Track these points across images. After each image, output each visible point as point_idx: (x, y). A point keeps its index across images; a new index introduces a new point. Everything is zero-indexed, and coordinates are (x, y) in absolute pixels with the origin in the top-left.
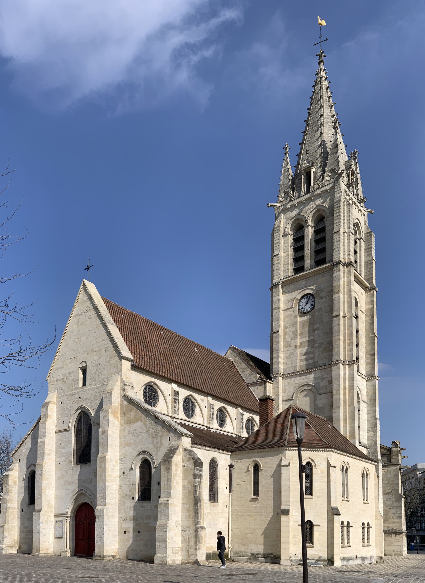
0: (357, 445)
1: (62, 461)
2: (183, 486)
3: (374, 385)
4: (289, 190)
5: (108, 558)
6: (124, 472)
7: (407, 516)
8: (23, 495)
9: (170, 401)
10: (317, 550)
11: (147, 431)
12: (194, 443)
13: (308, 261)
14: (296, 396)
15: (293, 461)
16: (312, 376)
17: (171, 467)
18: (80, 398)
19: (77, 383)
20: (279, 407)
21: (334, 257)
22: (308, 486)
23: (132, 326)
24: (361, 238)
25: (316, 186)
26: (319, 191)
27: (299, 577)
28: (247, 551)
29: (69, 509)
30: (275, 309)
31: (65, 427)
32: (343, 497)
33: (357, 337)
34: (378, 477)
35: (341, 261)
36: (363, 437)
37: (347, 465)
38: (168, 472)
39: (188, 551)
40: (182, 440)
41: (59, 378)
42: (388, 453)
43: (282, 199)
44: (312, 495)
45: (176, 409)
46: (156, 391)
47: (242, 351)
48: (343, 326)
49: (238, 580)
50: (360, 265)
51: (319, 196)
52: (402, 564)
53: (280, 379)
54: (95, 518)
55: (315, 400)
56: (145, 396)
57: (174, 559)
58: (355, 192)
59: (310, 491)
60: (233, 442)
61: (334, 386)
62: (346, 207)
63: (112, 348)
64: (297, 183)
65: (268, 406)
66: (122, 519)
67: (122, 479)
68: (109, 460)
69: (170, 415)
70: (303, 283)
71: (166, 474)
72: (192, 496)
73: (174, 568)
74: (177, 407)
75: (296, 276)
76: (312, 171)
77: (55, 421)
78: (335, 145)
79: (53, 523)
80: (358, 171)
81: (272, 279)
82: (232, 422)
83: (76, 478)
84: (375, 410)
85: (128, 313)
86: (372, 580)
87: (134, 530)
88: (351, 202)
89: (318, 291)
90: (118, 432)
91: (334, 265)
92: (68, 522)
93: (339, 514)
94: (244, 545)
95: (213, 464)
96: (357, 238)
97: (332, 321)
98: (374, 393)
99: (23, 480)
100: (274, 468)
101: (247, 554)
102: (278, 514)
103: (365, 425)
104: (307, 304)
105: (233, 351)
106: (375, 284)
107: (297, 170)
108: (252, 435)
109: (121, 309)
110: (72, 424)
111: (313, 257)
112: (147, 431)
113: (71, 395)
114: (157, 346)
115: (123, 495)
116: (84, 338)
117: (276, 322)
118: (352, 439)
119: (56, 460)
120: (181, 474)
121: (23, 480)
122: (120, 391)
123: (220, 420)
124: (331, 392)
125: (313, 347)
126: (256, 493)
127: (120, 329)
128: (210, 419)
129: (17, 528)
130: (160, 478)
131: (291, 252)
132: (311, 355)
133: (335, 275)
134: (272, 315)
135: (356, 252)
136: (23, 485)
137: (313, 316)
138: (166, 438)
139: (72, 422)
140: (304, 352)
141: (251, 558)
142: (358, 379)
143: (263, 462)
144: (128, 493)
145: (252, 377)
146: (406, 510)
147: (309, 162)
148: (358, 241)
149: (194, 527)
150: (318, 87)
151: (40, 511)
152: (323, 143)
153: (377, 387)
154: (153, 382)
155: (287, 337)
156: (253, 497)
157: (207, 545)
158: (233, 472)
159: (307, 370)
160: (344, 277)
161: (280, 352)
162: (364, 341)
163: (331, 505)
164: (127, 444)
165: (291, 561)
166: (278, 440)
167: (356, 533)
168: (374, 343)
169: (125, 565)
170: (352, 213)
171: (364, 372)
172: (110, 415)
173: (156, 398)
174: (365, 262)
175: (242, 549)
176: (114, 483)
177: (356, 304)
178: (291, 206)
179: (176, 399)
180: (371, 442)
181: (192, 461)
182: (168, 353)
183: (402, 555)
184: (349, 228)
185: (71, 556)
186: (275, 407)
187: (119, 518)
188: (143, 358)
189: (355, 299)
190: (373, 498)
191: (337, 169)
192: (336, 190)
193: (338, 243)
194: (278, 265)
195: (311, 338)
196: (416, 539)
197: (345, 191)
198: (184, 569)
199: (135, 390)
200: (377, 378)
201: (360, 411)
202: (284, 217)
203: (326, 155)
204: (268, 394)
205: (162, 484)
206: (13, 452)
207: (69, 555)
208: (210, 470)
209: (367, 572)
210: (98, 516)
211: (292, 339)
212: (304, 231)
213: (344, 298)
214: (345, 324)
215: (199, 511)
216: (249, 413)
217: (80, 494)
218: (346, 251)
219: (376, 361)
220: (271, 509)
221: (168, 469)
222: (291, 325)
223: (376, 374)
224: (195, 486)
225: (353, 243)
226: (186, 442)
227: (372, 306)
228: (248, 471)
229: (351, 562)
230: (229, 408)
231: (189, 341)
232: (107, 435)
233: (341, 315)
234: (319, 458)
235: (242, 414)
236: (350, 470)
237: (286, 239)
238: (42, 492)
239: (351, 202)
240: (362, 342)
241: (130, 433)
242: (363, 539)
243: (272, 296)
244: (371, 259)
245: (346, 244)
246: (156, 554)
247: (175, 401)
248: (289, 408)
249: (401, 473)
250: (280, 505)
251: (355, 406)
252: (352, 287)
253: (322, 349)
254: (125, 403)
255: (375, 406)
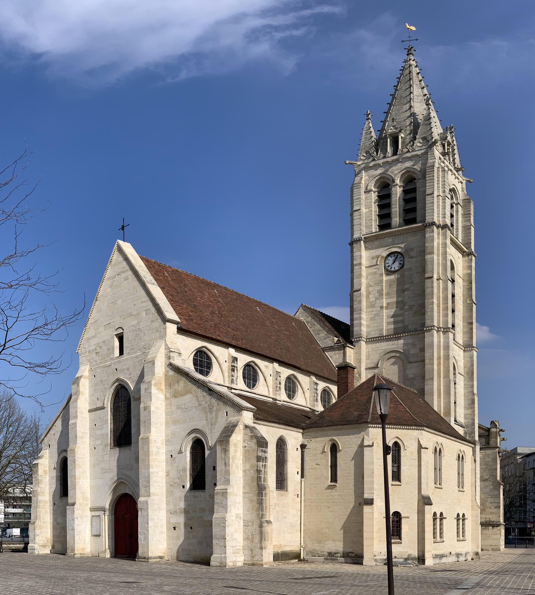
0: (452, 423)
1: (97, 445)
2: (244, 471)
3: (472, 357)
4: (373, 150)
5: (154, 560)
6: (172, 456)
7: (505, 506)
8: (54, 486)
9: (227, 369)
10: (406, 547)
11: (199, 405)
12: (257, 418)
13: (395, 219)
14: (382, 364)
15: (378, 441)
16: (401, 342)
17: (229, 448)
18: (116, 369)
19: (113, 353)
20: (362, 376)
21: (427, 218)
22: (395, 470)
23: (178, 284)
24: (458, 203)
25: (405, 150)
26: (408, 155)
27: (384, 579)
28: (322, 550)
29: (107, 502)
30: (356, 265)
31: (99, 405)
32: (435, 483)
33: (453, 302)
34: (475, 461)
35: (434, 222)
36: (459, 415)
37: (440, 446)
38: (225, 455)
39: (252, 550)
40: (242, 415)
41: (91, 348)
42: (487, 434)
43: (362, 158)
44: (400, 481)
45: (234, 378)
46: (209, 358)
47: (316, 311)
48: (437, 291)
49: (312, 584)
50: (457, 229)
51: (409, 159)
52: (500, 559)
53: (363, 344)
54: (137, 511)
55: (405, 369)
56: (195, 364)
57: (234, 560)
58: (451, 161)
59: (397, 476)
60: (306, 416)
61: (427, 355)
62: (440, 172)
63: (153, 310)
64: (381, 145)
65: (347, 374)
66: (171, 512)
67: (169, 464)
68: (153, 441)
69: (227, 385)
70: (390, 240)
71: (223, 456)
72: (256, 483)
73: (235, 571)
74: (235, 376)
75: (381, 233)
76: (400, 137)
77: (88, 398)
78: (428, 118)
79: (90, 518)
80: (455, 143)
81: (352, 235)
82: (304, 392)
83: (114, 464)
84: (473, 385)
85: (173, 271)
86: (466, 579)
87: (186, 525)
88: (446, 169)
89: (408, 250)
90: (163, 407)
91: (426, 226)
92: (106, 517)
93: (431, 504)
94: (320, 542)
95: (281, 444)
96: (454, 203)
97: (424, 282)
98: (472, 365)
99: (54, 469)
100: (355, 448)
101: (323, 553)
102: (360, 504)
103: (461, 401)
104: (394, 262)
105: (304, 310)
106: (473, 250)
107: (381, 134)
108: (329, 408)
109: (164, 267)
110: (108, 401)
111: (402, 215)
112: (199, 405)
113: (105, 367)
114: (209, 305)
115: (171, 483)
116: (119, 302)
117: (357, 280)
118: (446, 416)
119: (90, 444)
120: (241, 457)
121: (54, 469)
122: (164, 359)
123: (290, 391)
124: (423, 361)
125: (402, 309)
126: (334, 478)
127: (162, 288)
128: (277, 389)
129: (49, 525)
130: (215, 462)
131: (375, 209)
132: (400, 318)
133: (427, 235)
134: (352, 272)
135: (452, 216)
136: (55, 475)
137: (402, 276)
138: (223, 413)
139: (108, 398)
140: (392, 313)
141: (328, 558)
142: (455, 349)
143: (342, 441)
144: (177, 481)
145: (328, 340)
146: (504, 499)
147: (397, 128)
148: (454, 205)
149: (259, 522)
150: (407, 71)
151: (73, 504)
152: (413, 115)
153: (475, 359)
154: (205, 347)
155: (371, 296)
156: (330, 483)
157: (275, 543)
158: (305, 454)
159: (395, 335)
160: (438, 238)
161: (362, 312)
162: (461, 307)
163: (422, 493)
164: (176, 422)
165: (376, 560)
166: (360, 415)
167: (450, 525)
168: (472, 309)
169: (176, 568)
170: (447, 179)
171: (461, 341)
172: (152, 387)
173: (209, 366)
174: (462, 227)
175: (317, 547)
176: (160, 469)
177: (452, 268)
178: (374, 165)
179: (234, 366)
180: (468, 420)
181: (255, 441)
182: (224, 313)
183: (500, 550)
184: (444, 192)
185: (111, 557)
186: (357, 375)
187: (167, 511)
188: (192, 320)
189: (450, 263)
190: (470, 485)
191: (430, 138)
192: (429, 156)
193: (431, 205)
194: (358, 220)
195: (400, 299)
196: (515, 531)
197: (440, 159)
198: (248, 572)
199: (183, 357)
200: (475, 349)
201: (457, 385)
202: (366, 174)
203: (417, 125)
204: (348, 361)
205: (218, 468)
206: (43, 437)
207: (108, 555)
208: (277, 452)
209: (461, 571)
210: (141, 509)
211: (377, 299)
212: (390, 190)
213: (438, 260)
214: (439, 287)
215: (264, 501)
216: (324, 382)
217: (120, 483)
218: (441, 213)
219: (474, 330)
220: (352, 499)
221: (226, 451)
222: (375, 284)
223: (474, 345)
224: (259, 471)
225: (448, 207)
226: (247, 417)
227: (470, 272)
228: (324, 452)
229: (444, 560)
230: (300, 377)
231: (249, 299)
232: (149, 412)
233: (435, 276)
234: (409, 438)
235: (317, 384)
236: (445, 452)
237: (369, 195)
238: (75, 482)
239: (446, 169)
240: (459, 308)
241: (178, 408)
242: (458, 533)
243: (352, 252)
244: (469, 224)
245: (441, 207)
246: (212, 554)
247: (233, 369)
248: (373, 377)
249: (500, 457)
250: (363, 493)
251: (450, 378)
252: (448, 250)
253: (413, 312)
254: (171, 373)
255: (473, 380)
